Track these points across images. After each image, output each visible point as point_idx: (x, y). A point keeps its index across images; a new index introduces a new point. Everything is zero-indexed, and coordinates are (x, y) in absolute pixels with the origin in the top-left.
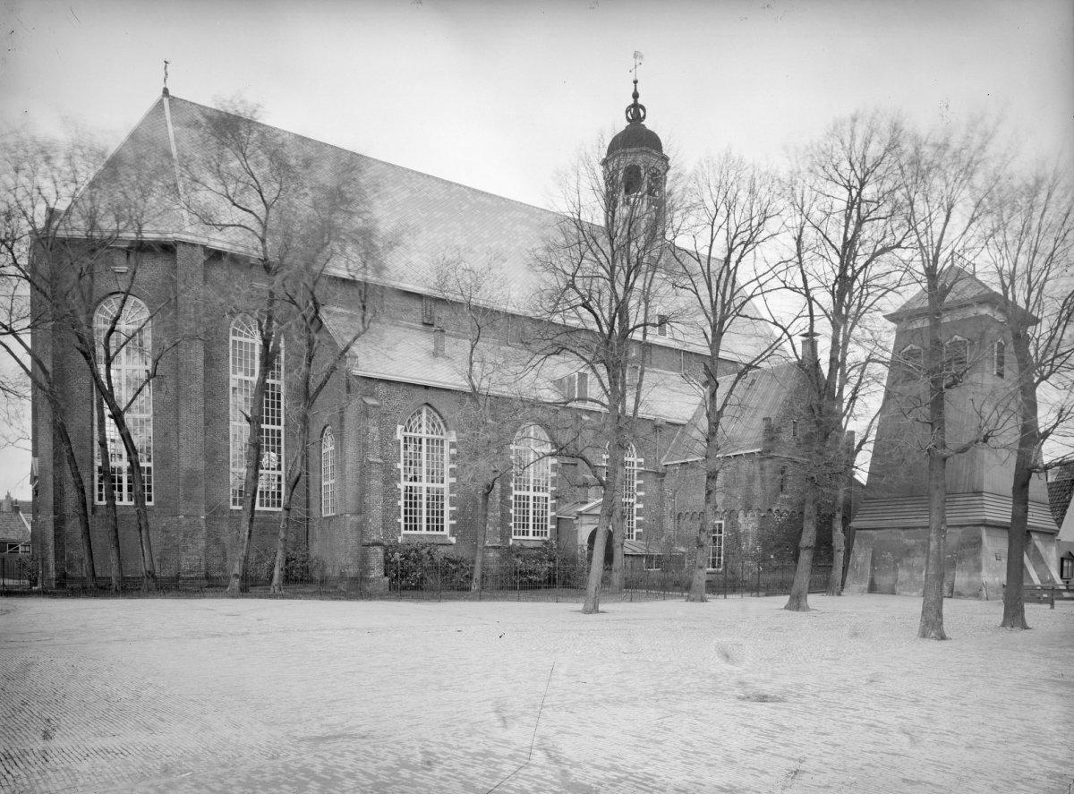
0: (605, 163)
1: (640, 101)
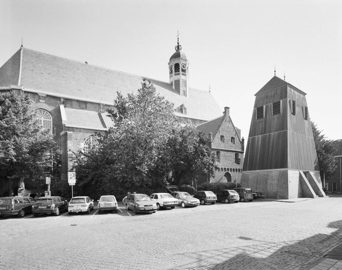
0: (169, 64)
1: (179, 44)
